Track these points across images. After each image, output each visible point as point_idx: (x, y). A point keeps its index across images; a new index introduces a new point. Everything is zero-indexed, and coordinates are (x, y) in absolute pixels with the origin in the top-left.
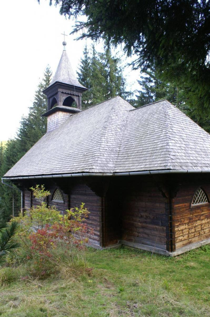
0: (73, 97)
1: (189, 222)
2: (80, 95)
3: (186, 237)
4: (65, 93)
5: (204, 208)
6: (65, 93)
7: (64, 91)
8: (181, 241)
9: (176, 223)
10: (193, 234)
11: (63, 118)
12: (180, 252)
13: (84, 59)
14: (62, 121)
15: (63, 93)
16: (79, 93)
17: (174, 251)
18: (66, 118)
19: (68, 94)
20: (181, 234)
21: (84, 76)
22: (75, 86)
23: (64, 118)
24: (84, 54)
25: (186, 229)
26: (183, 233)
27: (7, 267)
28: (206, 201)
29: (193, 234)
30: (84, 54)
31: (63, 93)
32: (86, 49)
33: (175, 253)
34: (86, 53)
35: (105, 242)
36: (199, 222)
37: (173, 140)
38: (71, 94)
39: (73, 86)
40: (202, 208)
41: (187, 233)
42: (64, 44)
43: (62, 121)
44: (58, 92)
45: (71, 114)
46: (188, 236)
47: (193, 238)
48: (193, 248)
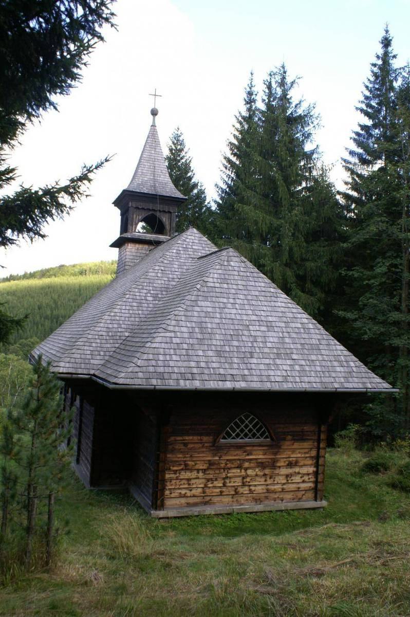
0: (158, 214)
1: (208, 469)
2: (172, 211)
3: (198, 492)
4: (143, 209)
5: (255, 448)
6: (143, 209)
7: (141, 205)
8: (181, 496)
9: (173, 466)
10: (218, 490)
11: (134, 254)
12: (171, 513)
13: (245, 114)
14: (133, 261)
15: (137, 208)
16: (171, 208)
17: (160, 510)
18: (142, 255)
19: (149, 210)
20: (186, 486)
21: (378, 96)
22: (160, 196)
23: (138, 255)
24: (247, 103)
25: (198, 478)
26: (189, 484)
27: (183, 536)
28: (267, 437)
29: (218, 490)
30: (247, 103)
31: (137, 208)
32: (250, 94)
33: (161, 513)
34: (250, 101)
35: (95, 480)
36: (239, 471)
37: (171, 331)
38: (154, 210)
39: (157, 195)
40: (248, 448)
41: (202, 486)
42: (154, 113)
43: (133, 261)
44: (129, 207)
45: (151, 247)
46: (204, 492)
47: (214, 497)
48: (207, 513)
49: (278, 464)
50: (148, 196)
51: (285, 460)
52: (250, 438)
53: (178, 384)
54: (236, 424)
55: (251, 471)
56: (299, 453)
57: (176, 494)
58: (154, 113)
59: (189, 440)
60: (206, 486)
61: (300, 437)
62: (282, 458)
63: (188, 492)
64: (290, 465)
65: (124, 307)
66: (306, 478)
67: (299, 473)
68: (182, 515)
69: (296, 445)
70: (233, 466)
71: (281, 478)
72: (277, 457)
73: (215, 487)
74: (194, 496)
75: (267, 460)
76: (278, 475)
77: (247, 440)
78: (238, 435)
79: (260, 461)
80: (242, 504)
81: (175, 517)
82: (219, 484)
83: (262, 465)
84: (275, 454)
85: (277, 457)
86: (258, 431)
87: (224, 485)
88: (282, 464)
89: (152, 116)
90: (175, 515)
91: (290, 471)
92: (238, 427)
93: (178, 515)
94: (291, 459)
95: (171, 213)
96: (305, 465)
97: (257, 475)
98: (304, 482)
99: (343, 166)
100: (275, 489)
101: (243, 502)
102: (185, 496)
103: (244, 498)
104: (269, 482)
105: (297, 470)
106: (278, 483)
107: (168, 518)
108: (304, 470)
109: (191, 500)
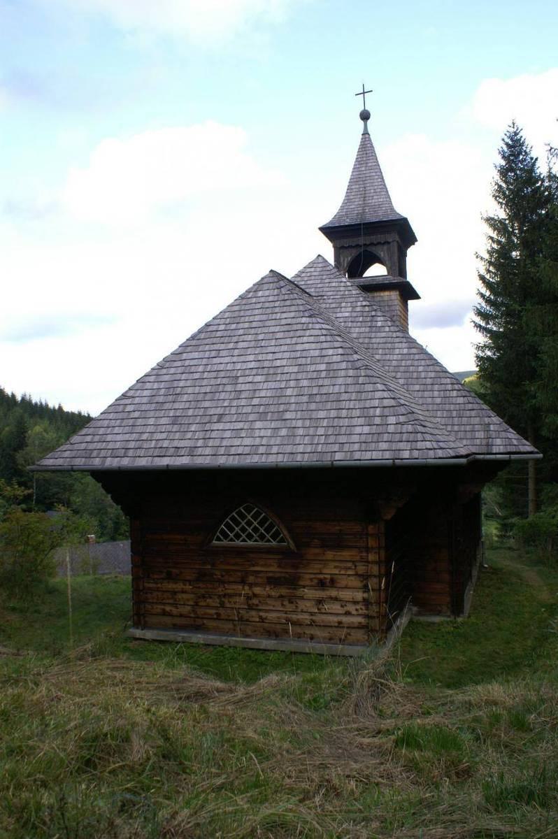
4: (350, 247)
6: (350, 247)
19: (358, 246)
22: (364, 224)
29: (213, 611)
40: (252, 555)
42: (365, 116)
49: (301, 583)
50: (351, 228)
51: (312, 576)
52: (256, 541)
53: (103, 463)
54: (233, 519)
55: (258, 588)
56: (335, 567)
57: (159, 611)
58: (365, 116)
59: (335, 609)
60: (196, 604)
61: (338, 543)
62: (308, 574)
63: (174, 609)
64: (322, 584)
65: (429, 400)
66: (351, 608)
67: (336, 599)
68: (162, 639)
69: (330, 555)
70: (232, 579)
71: (308, 604)
72: (299, 571)
73: (208, 606)
74: (181, 616)
75: (283, 575)
76: (302, 598)
77: (250, 543)
78: (238, 536)
79: (270, 575)
80: (247, 636)
81: (155, 640)
82: (214, 602)
83: (273, 581)
84: (295, 567)
85: (299, 571)
86: (238, 524)
87: (222, 605)
88: (308, 583)
89: (362, 122)
90: (155, 638)
91: (320, 594)
92: (238, 524)
93: (159, 638)
94: (322, 576)
95: (389, 243)
96: (346, 587)
97: (269, 596)
98: (348, 613)
99: (497, 184)
100: (298, 619)
101: (249, 633)
102: (170, 614)
103: (250, 627)
104: (290, 607)
105: (334, 593)
106: (302, 611)
107: (144, 640)
108: (346, 595)
109: (178, 621)
